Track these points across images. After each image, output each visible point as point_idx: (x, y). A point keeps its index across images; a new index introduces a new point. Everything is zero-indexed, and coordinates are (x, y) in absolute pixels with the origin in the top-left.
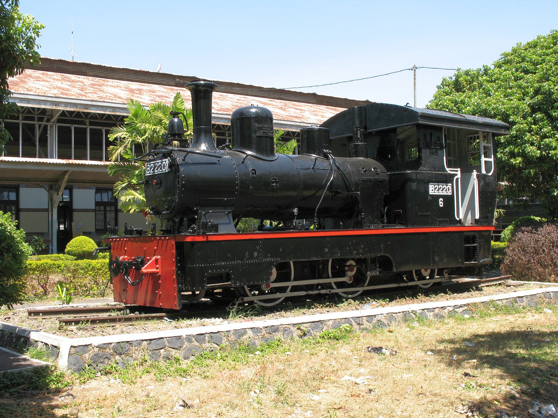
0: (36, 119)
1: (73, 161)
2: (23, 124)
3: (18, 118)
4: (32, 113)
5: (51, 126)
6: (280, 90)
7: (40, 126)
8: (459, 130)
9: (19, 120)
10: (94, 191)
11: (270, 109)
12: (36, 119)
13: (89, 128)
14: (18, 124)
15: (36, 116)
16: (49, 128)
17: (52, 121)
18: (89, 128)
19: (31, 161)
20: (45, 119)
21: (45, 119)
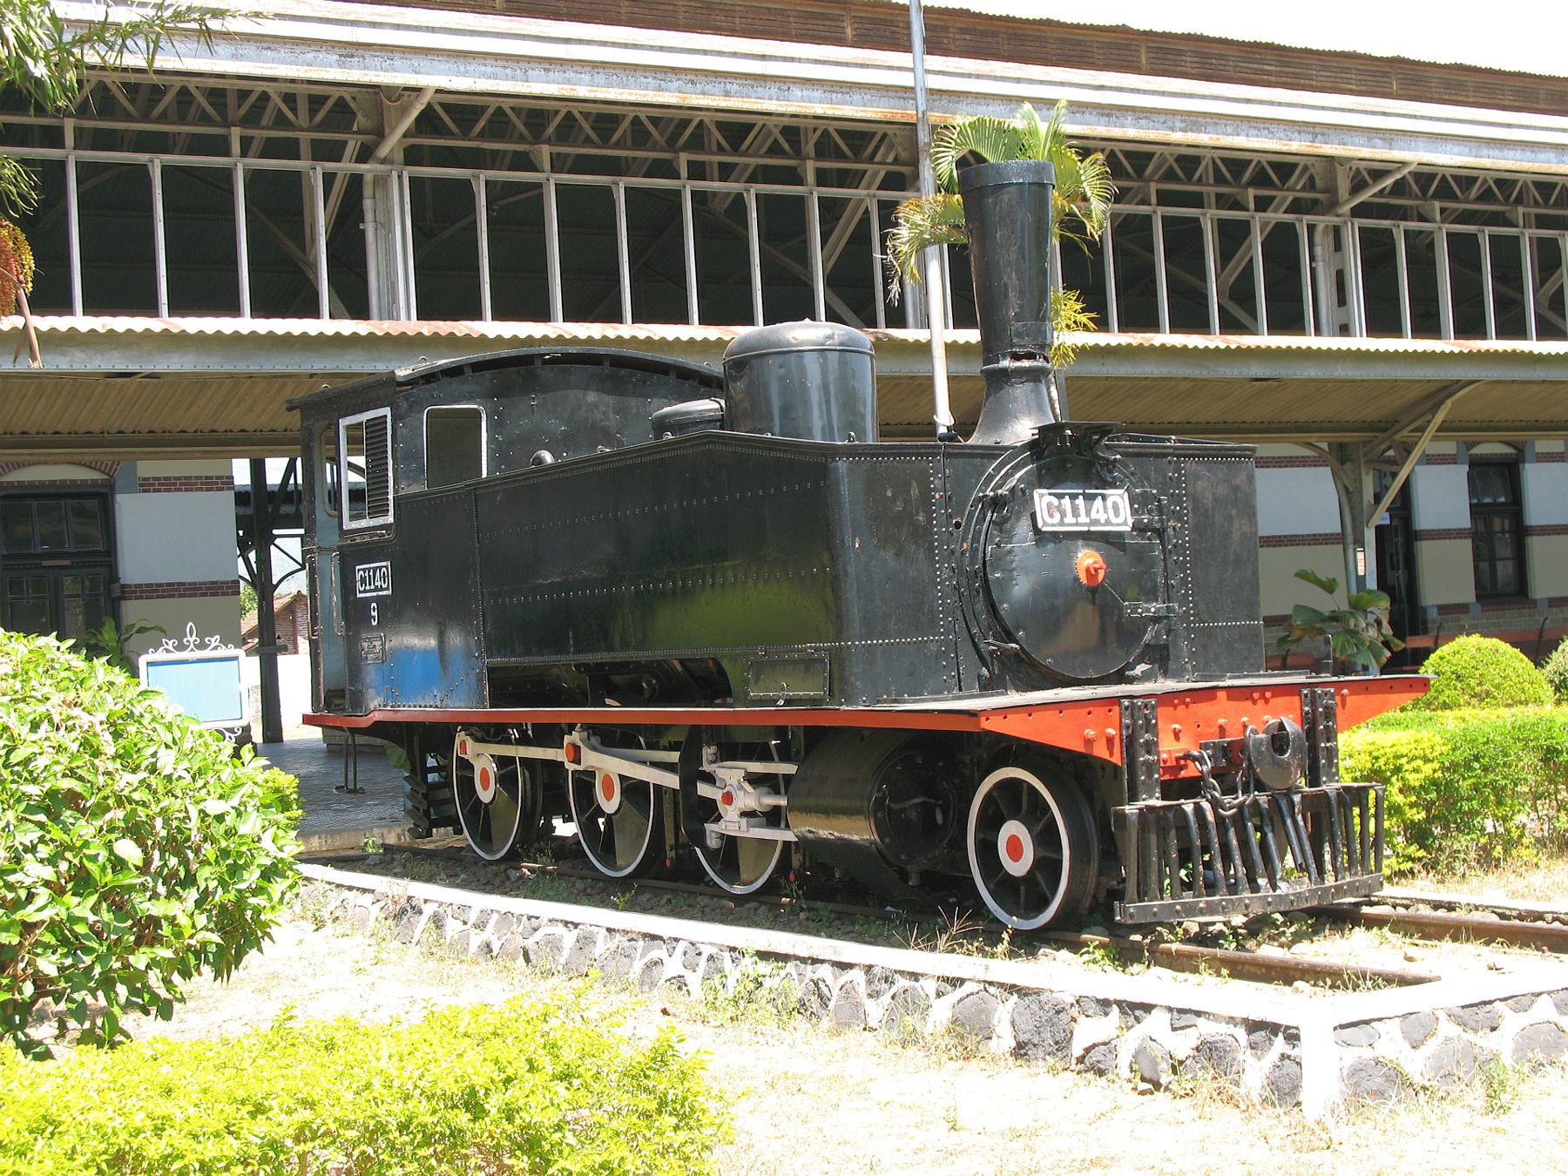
0: (305, 149)
1: (628, 330)
2: (254, 177)
3: (219, 146)
4: (287, 124)
5: (381, 182)
6: (1145, 33)
7: (329, 179)
8: (492, 151)
9: (61, 145)
10: (1466, 468)
11: (267, 90)
12: (305, 149)
13: (551, 182)
14: (227, 175)
15: (305, 137)
16: (368, 191)
17: (384, 151)
18: (551, 182)
19: (296, 332)
20: (351, 148)
21: (351, 148)
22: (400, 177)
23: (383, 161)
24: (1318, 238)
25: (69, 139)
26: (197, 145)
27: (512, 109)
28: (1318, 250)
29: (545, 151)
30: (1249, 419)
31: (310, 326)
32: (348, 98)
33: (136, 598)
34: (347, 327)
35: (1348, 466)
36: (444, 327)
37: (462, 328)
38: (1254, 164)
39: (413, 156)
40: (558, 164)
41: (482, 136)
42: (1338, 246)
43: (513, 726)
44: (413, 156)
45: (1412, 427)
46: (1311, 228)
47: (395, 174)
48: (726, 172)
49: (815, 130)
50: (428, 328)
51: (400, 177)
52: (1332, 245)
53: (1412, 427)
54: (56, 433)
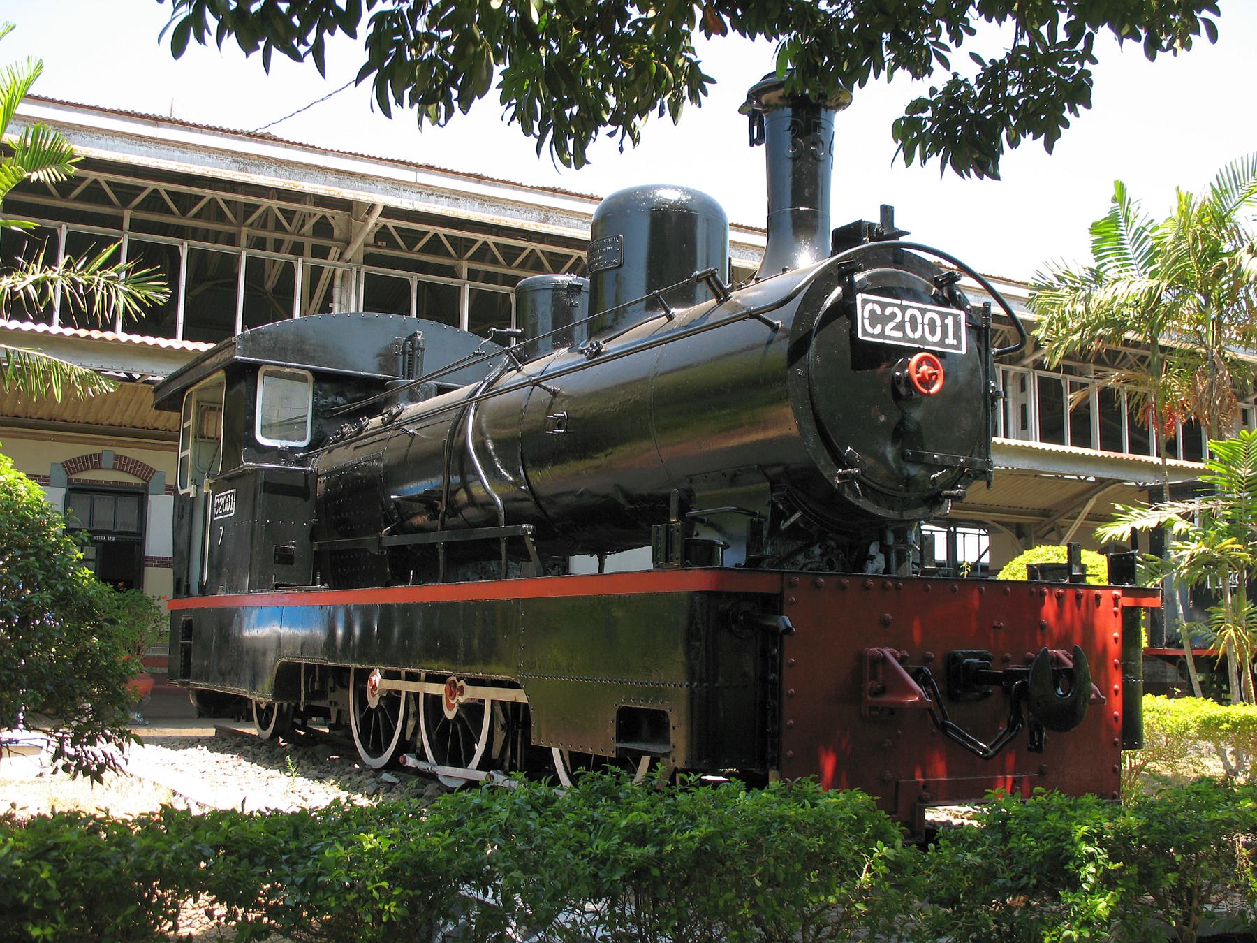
10: (63, 491)
22: (358, 272)
23: (349, 261)
24: (1010, 381)
25: (126, 225)
26: (216, 237)
27: (107, 182)
28: (1009, 388)
29: (127, 215)
30: (978, 501)
31: (1060, 448)
32: (328, 216)
33: (156, 566)
34: (1020, 443)
35: (1023, 540)
36: (1137, 457)
37: (1144, 458)
38: (261, 210)
39: (369, 259)
40: (473, 275)
41: (422, 251)
42: (1023, 388)
43: (1228, 686)
44: (369, 259)
45: (1067, 515)
46: (1005, 373)
47: (355, 270)
48: (278, 246)
49: (315, 215)
50: (1106, 454)
51: (358, 272)
52: (1019, 388)
53: (1067, 515)
54: (156, 429)
